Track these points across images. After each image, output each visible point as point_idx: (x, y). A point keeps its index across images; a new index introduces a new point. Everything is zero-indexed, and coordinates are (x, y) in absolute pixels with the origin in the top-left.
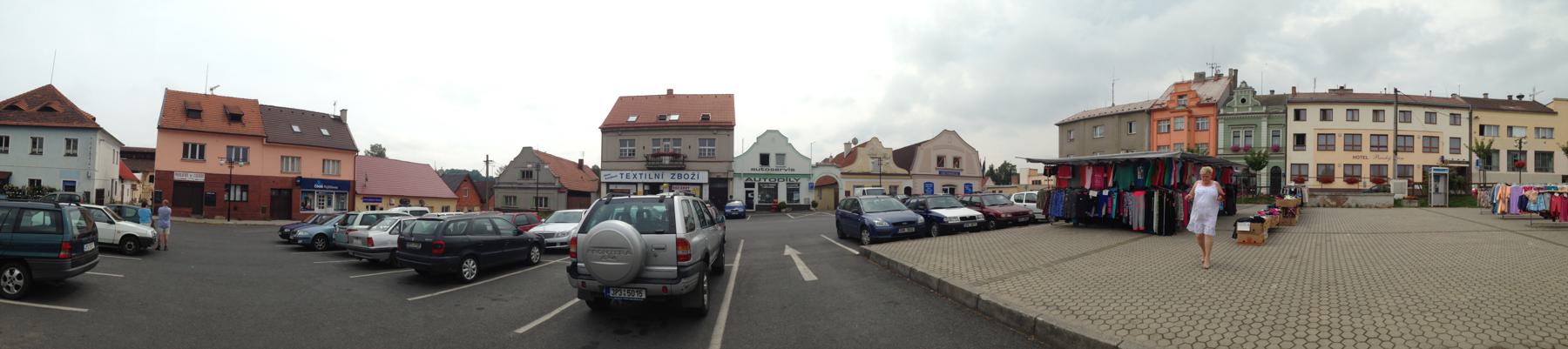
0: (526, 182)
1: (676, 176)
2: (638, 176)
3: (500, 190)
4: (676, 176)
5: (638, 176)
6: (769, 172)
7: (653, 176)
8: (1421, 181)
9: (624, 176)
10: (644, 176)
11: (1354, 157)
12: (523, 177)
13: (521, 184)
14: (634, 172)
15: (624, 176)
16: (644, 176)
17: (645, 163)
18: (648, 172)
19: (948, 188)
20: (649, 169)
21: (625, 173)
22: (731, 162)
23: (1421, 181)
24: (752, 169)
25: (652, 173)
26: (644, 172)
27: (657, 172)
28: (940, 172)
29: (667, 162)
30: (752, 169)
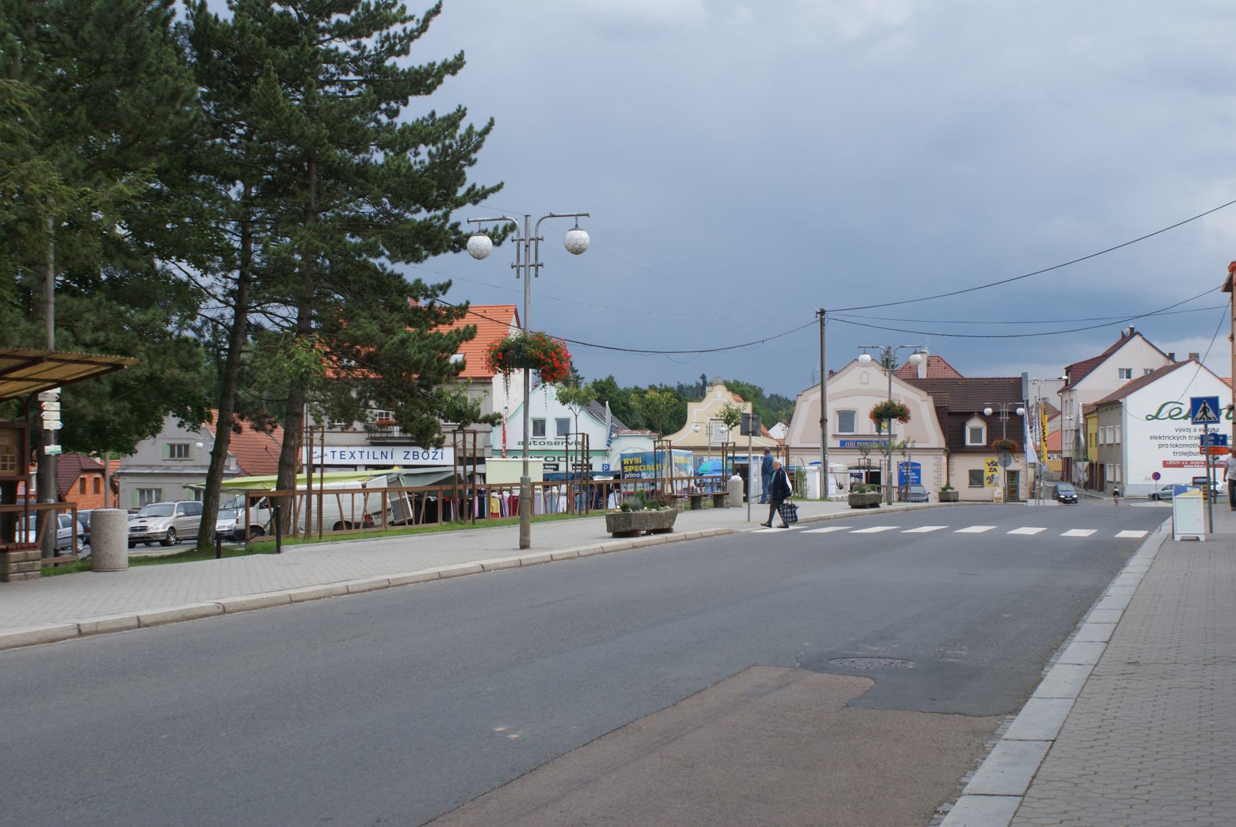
0: (178, 466)
1: (410, 456)
2: (357, 455)
3: (129, 479)
4: (410, 456)
5: (357, 455)
6: (546, 447)
7: (378, 455)
8: (1205, 470)
9: (337, 455)
10: (365, 455)
11: (1091, 446)
12: (172, 455)
13: (168, 467)
14: (352, 449)
15: (337, 455)
16: (365, 455)
17: (366, 435)
18: (371, 449)
19: (863, 472)
20: (373, 444)
21: (338, 449)
22: (489, 432)
23: (897, 485)
24: (518, 277)
25: (378, 450)
26: (366, 449)
27: (384, 449)
28: (842, 443)
29: (397, 434)
30: (518, 277)
